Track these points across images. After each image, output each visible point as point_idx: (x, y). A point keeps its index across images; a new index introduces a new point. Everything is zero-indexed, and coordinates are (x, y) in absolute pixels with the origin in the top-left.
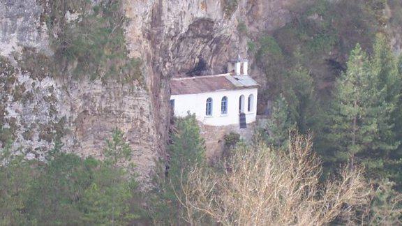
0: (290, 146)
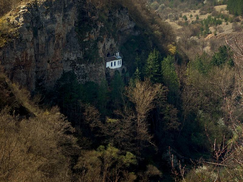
0: (201, 72)
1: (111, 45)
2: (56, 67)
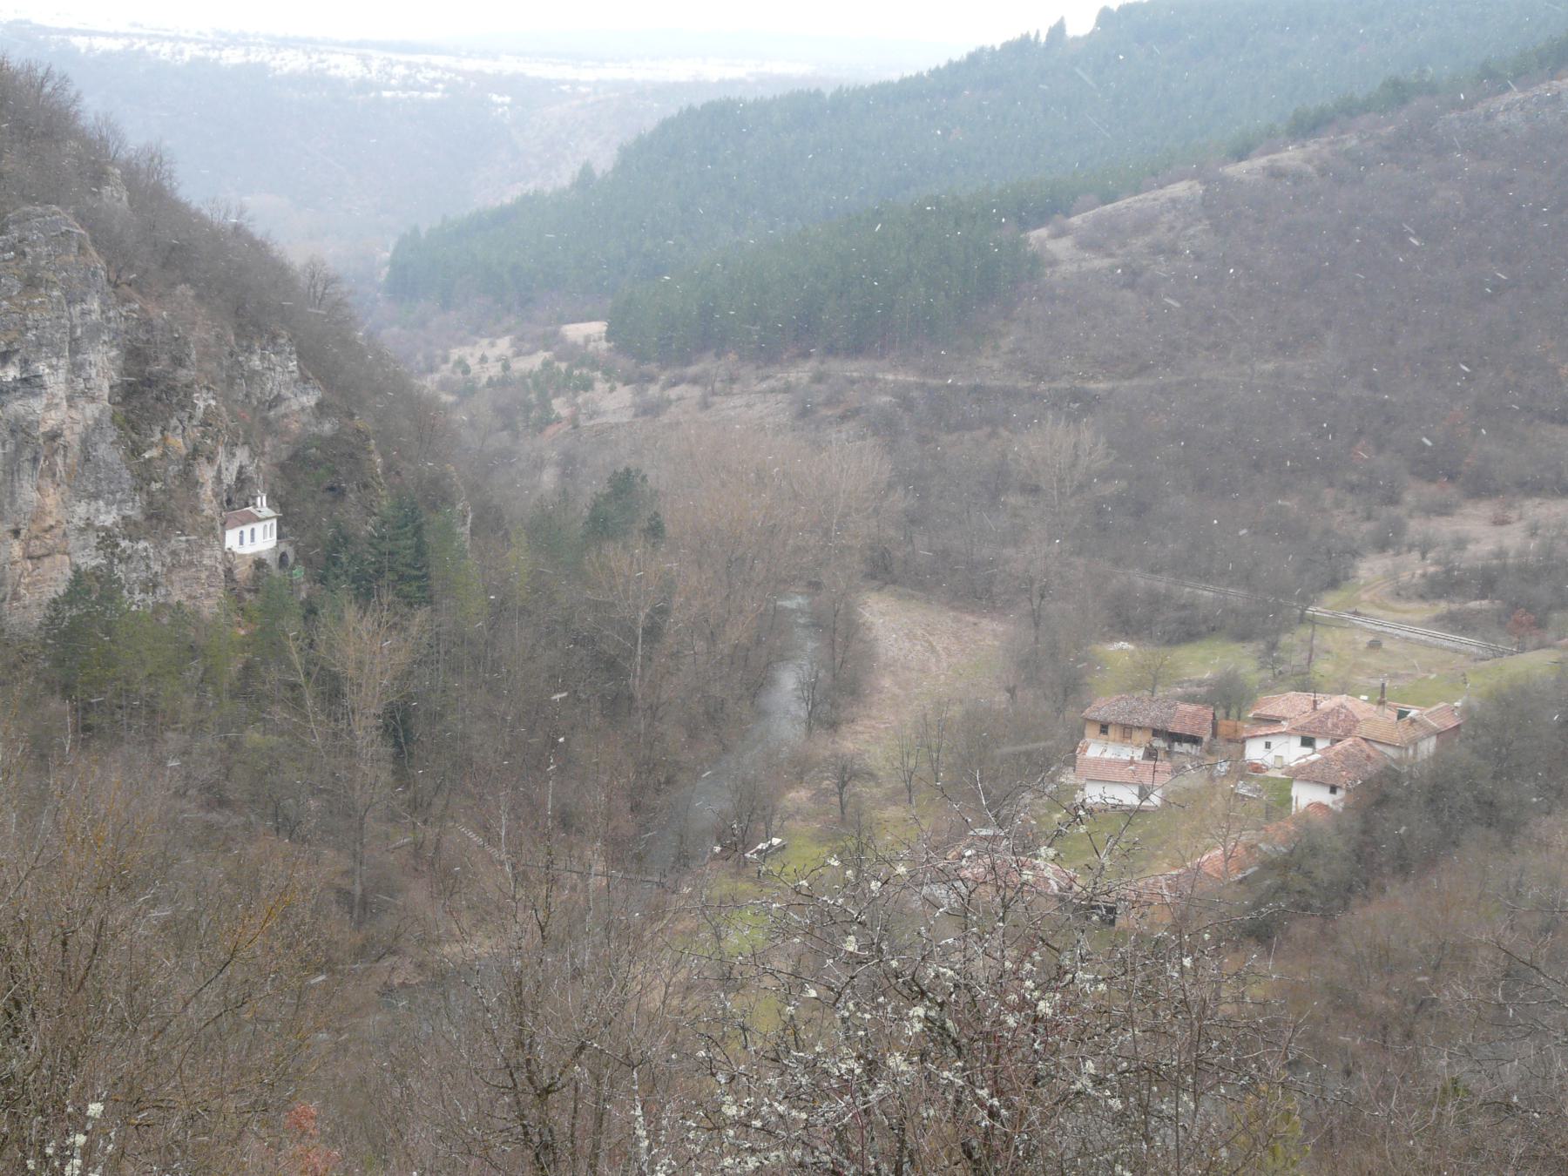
1: (241, 469)
2: (43, 551)
